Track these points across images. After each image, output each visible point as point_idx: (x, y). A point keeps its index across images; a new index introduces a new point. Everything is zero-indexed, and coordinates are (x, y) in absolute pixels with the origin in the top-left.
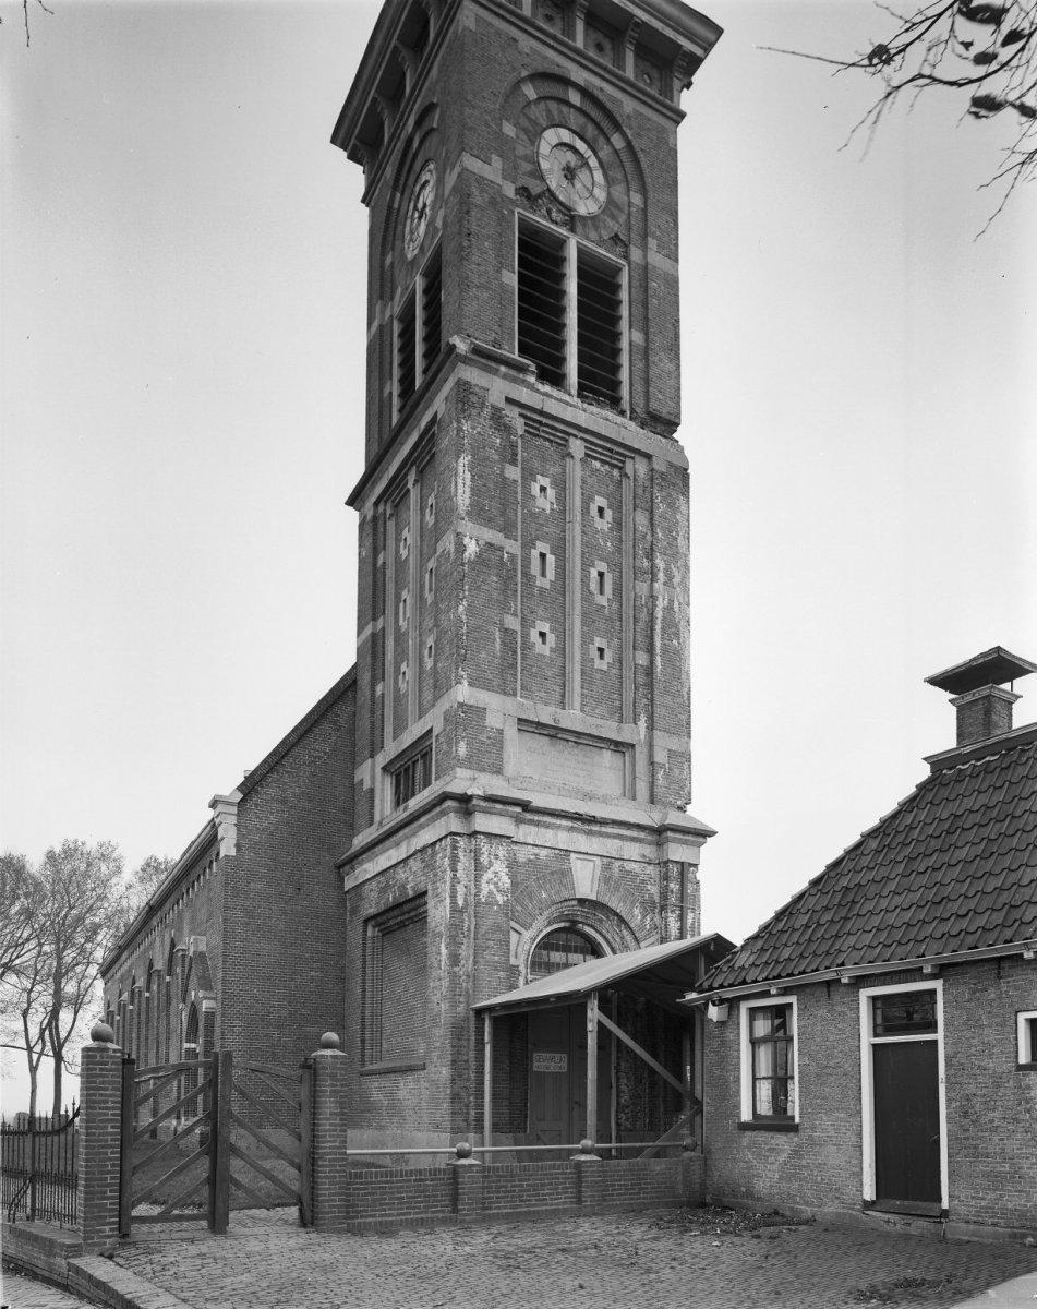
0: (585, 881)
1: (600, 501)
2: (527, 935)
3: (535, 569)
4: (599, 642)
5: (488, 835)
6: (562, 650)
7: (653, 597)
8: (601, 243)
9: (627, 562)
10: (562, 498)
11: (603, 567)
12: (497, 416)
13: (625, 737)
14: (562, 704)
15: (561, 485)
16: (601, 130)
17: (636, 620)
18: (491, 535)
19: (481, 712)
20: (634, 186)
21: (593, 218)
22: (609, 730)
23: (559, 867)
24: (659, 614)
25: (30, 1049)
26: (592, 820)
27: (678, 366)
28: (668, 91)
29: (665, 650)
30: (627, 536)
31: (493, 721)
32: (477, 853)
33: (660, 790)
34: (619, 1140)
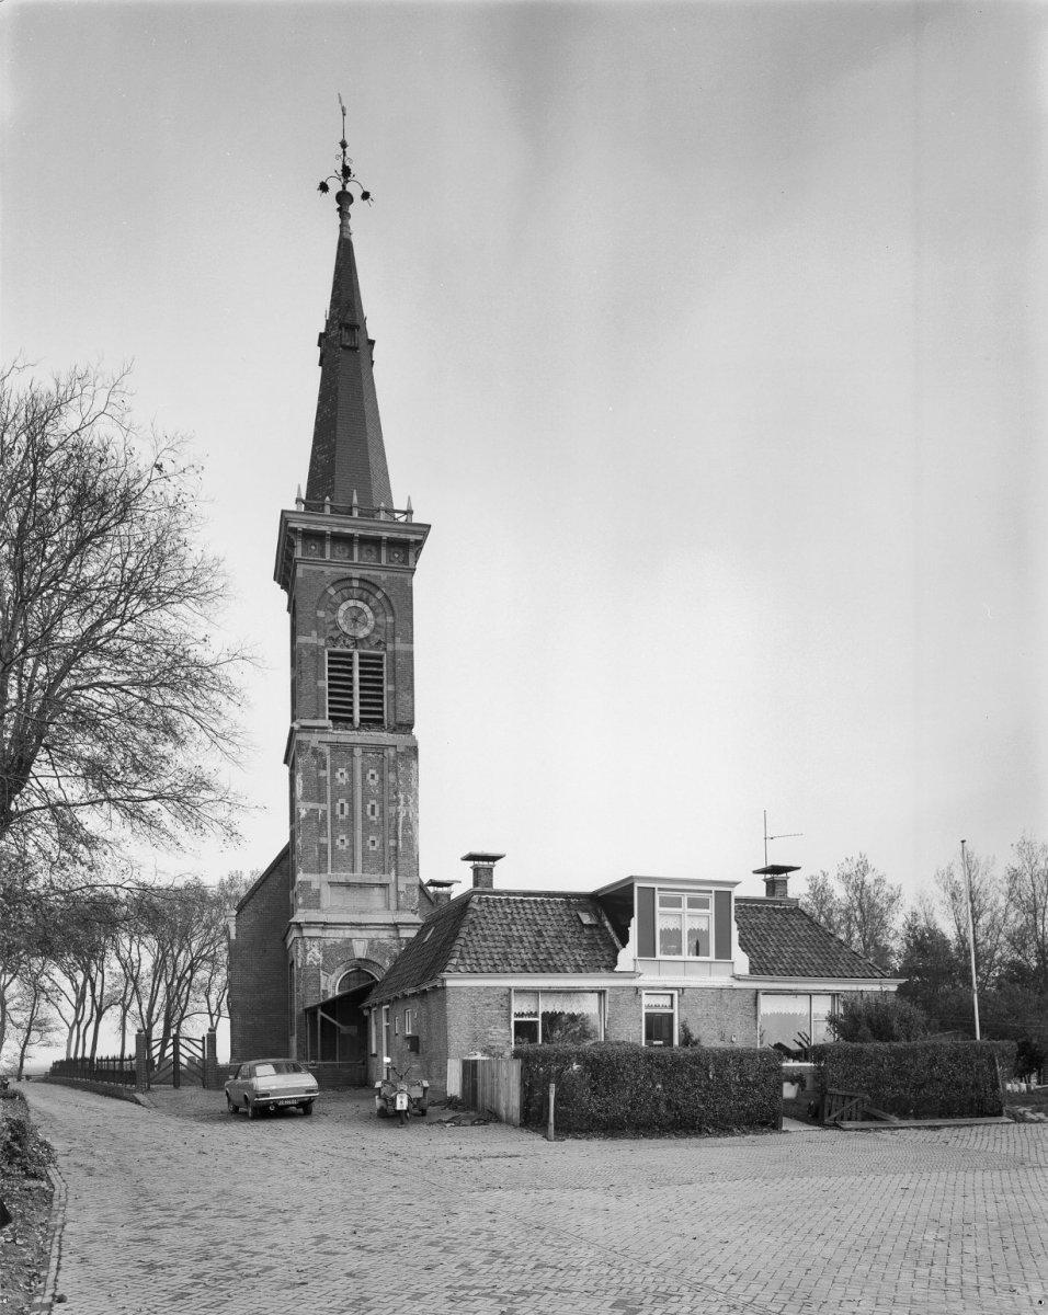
0: (360, 950)
1: (372, 772)
2: (333, 977)
3: (338, 812)
4: (371, 838)
5: (310, 938)
6: (352, 846)
7: (397, 813)
8: (371, 648)
9: (386, 798)
10: (352, 776)
11: (373, 802)
12: (315, 752)
13: (384, 881)
14: (353, 871)
15: (351, 770)
16: (371, 593)
17: (390, 825)
18: (311, 805)
19: (309, 883)
20: (389, 612)
21: (367, 638)
22: (375, 878)
23: (347, 946)
24: (401, 820)
25: (211, 1015)
26: (360, 924)
27: (413, 696)
28: (406, 561)
29: (404, 837)
30: (386, 784)
31: (315, 886)
32: (305, 946)
33: (401, 904)
34: (323, 1059)
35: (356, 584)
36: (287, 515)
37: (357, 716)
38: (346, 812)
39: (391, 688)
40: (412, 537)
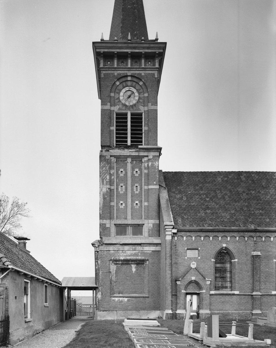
15: (126, 170)
35: (129, 78)
36: (97, 45)
37: (129, 143)
38: (139, 190)
39: (112, 128)
40: (157, 51)
